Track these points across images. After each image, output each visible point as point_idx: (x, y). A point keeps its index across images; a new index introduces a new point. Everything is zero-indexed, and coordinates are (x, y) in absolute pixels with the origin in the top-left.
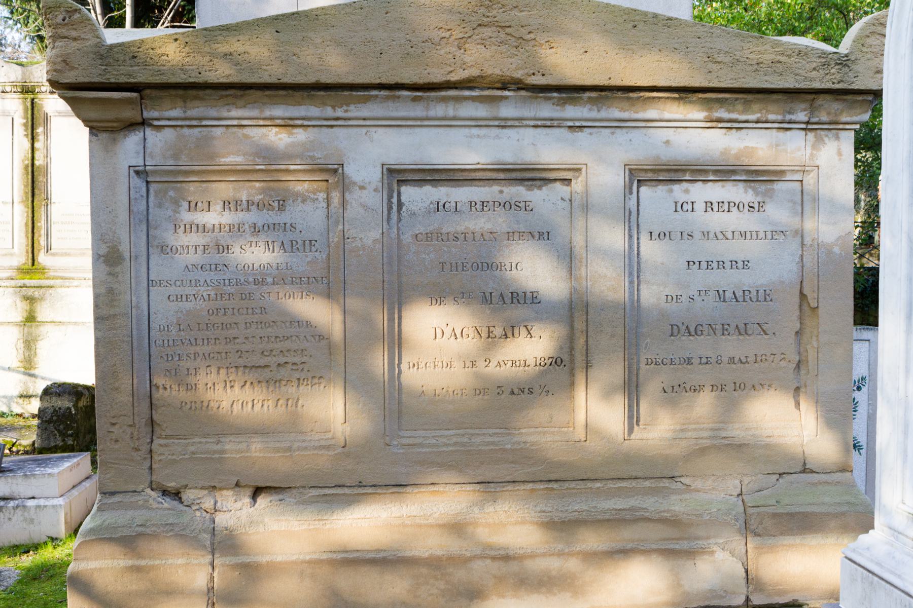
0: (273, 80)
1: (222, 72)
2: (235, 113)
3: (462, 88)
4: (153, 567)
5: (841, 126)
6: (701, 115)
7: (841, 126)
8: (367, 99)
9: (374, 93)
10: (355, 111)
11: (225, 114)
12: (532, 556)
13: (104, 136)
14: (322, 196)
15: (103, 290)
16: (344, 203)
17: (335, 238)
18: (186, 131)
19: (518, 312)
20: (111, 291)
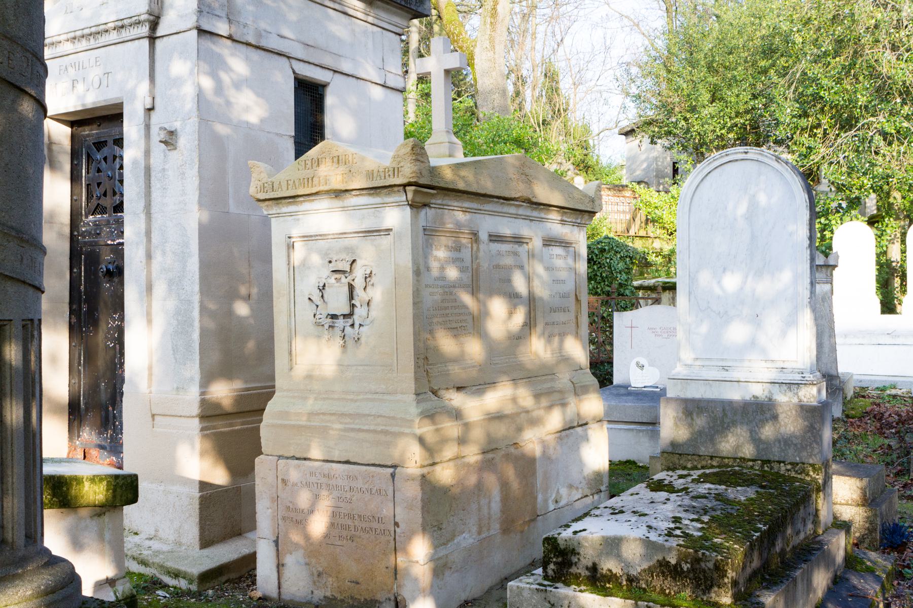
0: (475, 191)
1: (461, 186)
2: (456, 204)
3: (517, 201)
4: (442, 428)
5: (452, 208)
6: (559, 218)
7: (452, 208)
8: (489, 202)
9: (495, 200)
10: (506, 209)
11: (450, 203)
12: (533, 411)
13: (415, 209)
14: (470, 245)
15: (415, 289)
16: (478, 249)
17: (475, 267)
18: (438, 211)
19: (516, 300)
20: (418, 289)
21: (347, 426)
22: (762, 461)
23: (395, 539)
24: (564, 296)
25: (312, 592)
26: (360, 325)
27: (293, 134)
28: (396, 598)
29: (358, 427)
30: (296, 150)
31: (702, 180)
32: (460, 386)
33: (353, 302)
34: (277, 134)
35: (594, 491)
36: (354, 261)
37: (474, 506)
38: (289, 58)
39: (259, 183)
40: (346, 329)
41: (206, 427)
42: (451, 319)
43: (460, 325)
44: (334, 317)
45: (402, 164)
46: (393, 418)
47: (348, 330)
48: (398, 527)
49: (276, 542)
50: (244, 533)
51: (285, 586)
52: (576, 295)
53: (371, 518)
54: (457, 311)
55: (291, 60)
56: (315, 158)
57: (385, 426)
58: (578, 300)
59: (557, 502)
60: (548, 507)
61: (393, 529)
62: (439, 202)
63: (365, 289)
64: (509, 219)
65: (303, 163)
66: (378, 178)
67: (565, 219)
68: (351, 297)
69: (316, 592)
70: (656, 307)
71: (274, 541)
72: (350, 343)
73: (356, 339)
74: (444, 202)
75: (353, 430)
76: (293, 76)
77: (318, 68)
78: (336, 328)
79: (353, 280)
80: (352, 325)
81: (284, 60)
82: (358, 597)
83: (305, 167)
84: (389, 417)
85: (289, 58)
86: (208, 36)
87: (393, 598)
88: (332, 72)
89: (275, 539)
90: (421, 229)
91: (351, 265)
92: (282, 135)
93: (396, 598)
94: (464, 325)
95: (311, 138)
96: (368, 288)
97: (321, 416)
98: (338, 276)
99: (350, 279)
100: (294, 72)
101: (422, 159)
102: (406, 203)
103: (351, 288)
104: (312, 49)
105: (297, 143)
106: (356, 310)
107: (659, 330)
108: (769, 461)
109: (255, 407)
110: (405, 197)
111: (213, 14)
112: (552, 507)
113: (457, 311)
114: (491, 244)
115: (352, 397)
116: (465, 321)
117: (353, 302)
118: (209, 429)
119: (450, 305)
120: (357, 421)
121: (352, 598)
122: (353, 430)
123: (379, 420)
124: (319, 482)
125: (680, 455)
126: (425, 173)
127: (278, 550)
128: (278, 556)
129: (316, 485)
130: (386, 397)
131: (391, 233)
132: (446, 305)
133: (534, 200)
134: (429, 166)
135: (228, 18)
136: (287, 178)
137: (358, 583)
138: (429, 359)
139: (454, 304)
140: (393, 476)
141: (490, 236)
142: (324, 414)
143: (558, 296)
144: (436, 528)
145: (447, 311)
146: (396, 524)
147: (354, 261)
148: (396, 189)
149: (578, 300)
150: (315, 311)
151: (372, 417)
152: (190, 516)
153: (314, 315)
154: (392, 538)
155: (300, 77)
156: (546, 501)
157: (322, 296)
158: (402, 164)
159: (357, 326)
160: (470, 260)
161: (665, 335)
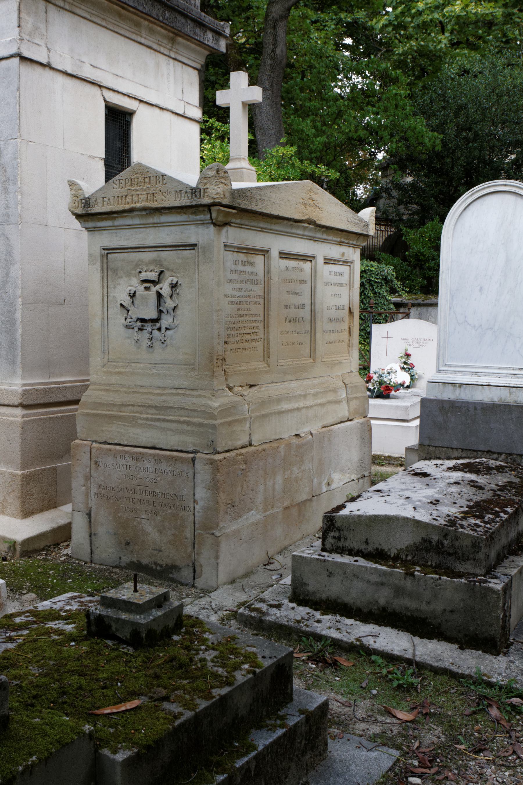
10: (117, 222)
13: (217, 227)
21: (153, 416)
22: (506, 454)
23: (194, 514)
24: (339, 308)
25: (120, 558)
26: (167, 329)
27: (104, 157)
28: (194, 564)
29: (163, 417)
30: (106, 171)
31: (465, 209)
32: (252, 384)
33: (161, 308)
34: (90, 157)
35: (359, 476)
36: (162, 272)
37: (261, 488)
38: (100, 86)
39: (76, 199)
40: (153, 331)
41: (27, 414)
42: (245, 325)
43: (253, 331)
44: (143, 321)
45: (207, 186)
46: (195, 410)
47: (156, 333)
48: (197, 504)
49: (89, 515)
50: (59, 506)
51: (96, 552)
52: (350, 308)
53: (173, 496)
54: (251, 318)
55: (102, 89)
56: (129, 177)
57: (188, 417)
58: (351, 312)
59: (329, 485)
60: (322, 489)
61: (192, 506)
62: (238, 221)
63: (171, 297)
64: (136, 230)
65: (117, 182)
66: (186, 198)
67: (343, 240)
68: (159, 304)
69: (123, 558)
70: (406, 321)
71: (87, 514)
72: (157, 344)
73: (163, 341)
74: (243, 222)
75: (159, 420)
76: (103, 104)
77: (126, 97)
78: (144, 331)
79: (161, 289)
80: (159, 329)
81: (96, 91)
82: (160, 562)
83: (120, 186)
84: (191, 410)
85: (100, 86)
86: (29, 63)
87: (191, 564)
88: (138, 102)
89: (88, 512)
90: (223, 245)
91: (159, 275)
92: (94, 158)
93: (194, 564)
94: (256, 331)
95: (119, 161)
96: (174, 296)
97: (130, 407)
98: (147, 285)
99: (158, 287)
100: (105, 100)
101: (226, 182)
102: (210, 221)
103: (159, 296)
104: (121, 79)
105: (108, 165)
106: (163, 316)
107: (410, 340)
108: (511, 454)
109: (75, 398)
110: (209, 216)
111: (33, 43)
112: (324, 489)
113: (251, 318)
114: (281, 260)
115: (158, 391)
116: (257, 327)
117: (161, 308)
118: (30, 416)
119: (245, 313)
120: (163, 412)
121: (155, 563)
122: (159, 420)
123: (182, 412)
124: (129, 464)
125: (436, 447)
126: (228, 195)
127: (90, 522)
128: (90, 527)
129: (125, 467)
130: (188, 392)
131: (196, 248)
132: (242, 313)
133: (318, 222)
134: (232, 189)
135: (46, 47)
136: (103, 196)
137: (160, 551)
138: (226, 360)
139: (248, 312)
140: (193, 460)
141: (280, 253)
142: (133, 405)
143: (335, 308)
144: (229, 506)
145: (242, 319)
146: (195, 501)
147: (162, 272)
148: (201, 209)
149: (351, 312)
150: (125, 315)
151: (176, 410)
152: (13, 491)
153: (126, 319)
154: (192, 513)
155: (110, 105)
156: (320, 484)
157: (133, 302)
158: (207, 186)
159: (163, 330)
160: (263, 275)
161: (416, 345)
